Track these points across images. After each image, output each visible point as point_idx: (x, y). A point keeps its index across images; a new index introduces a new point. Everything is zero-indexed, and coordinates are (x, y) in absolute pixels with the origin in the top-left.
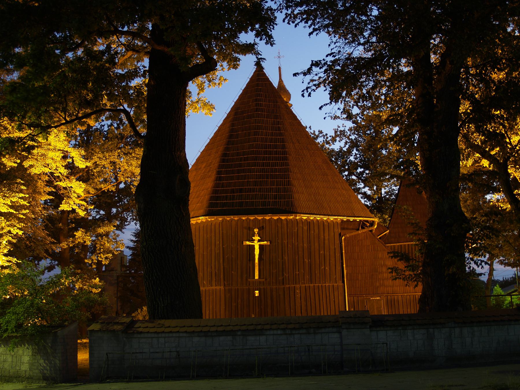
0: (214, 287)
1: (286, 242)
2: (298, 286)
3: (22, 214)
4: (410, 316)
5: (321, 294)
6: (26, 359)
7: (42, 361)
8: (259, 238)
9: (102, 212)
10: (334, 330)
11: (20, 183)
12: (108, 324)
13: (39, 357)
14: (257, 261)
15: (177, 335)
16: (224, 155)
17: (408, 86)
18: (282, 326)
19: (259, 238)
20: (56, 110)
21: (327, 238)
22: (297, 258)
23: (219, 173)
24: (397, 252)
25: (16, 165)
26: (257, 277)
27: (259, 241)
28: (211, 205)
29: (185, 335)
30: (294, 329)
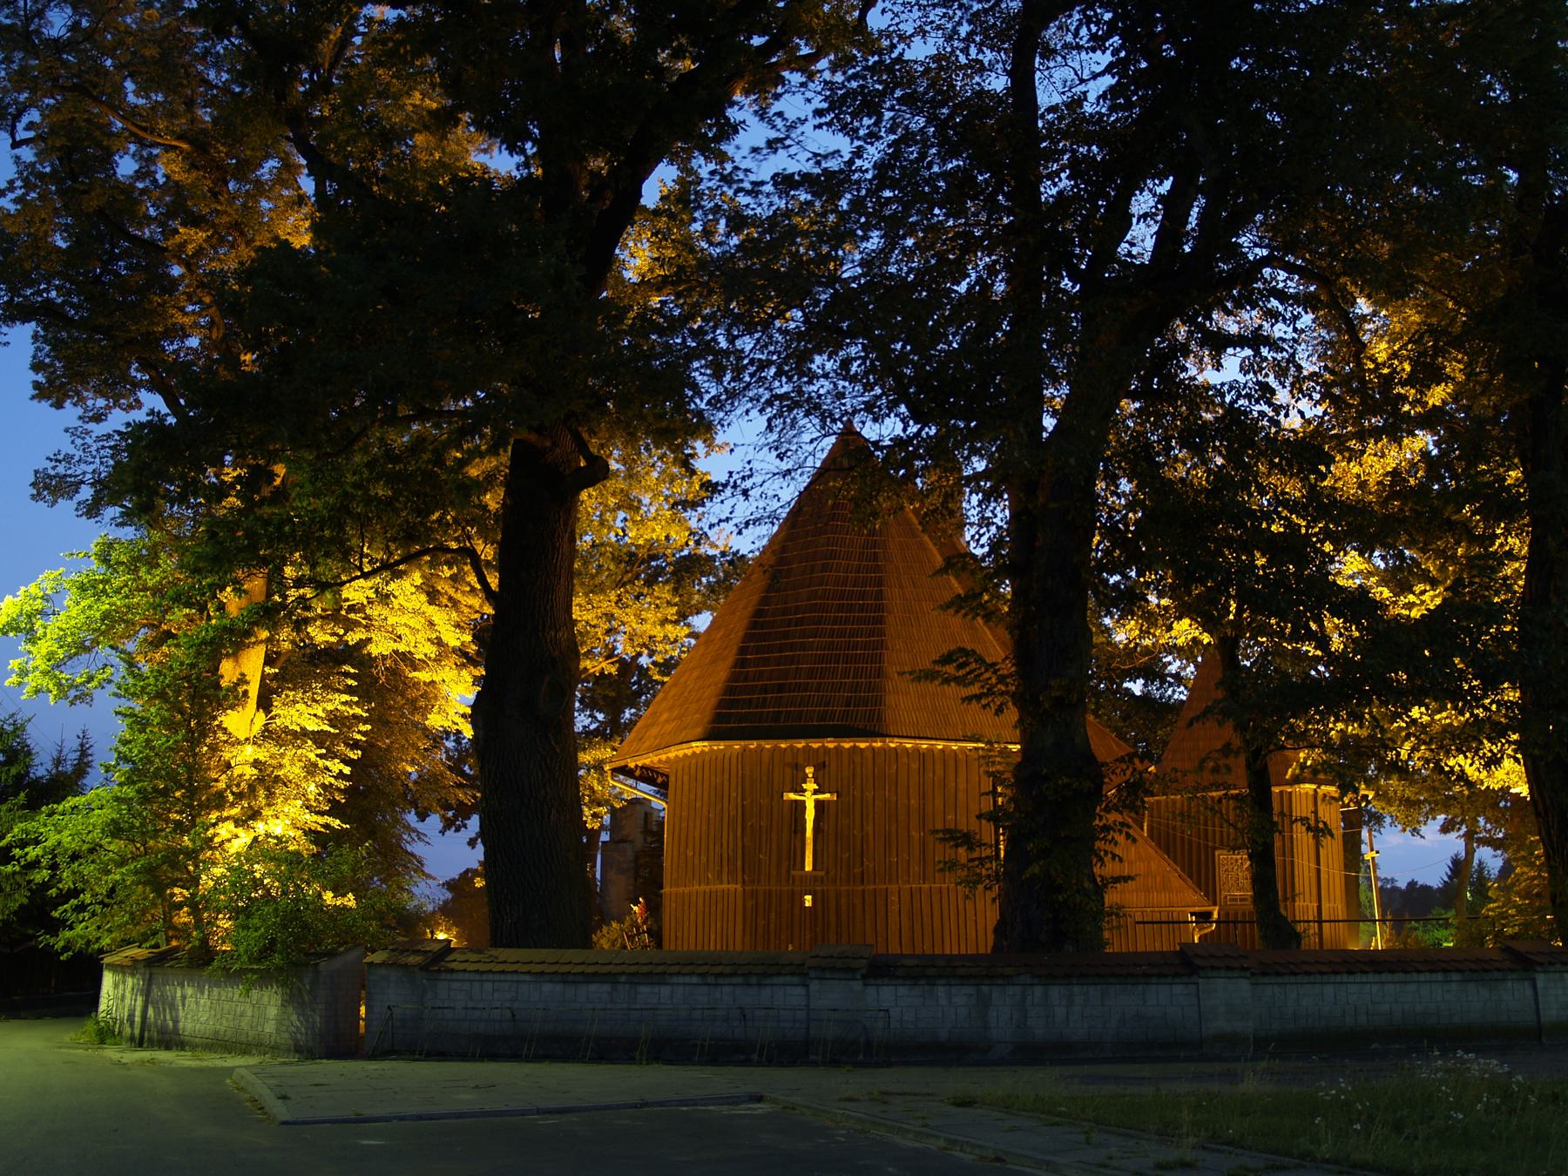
0: (725, 886)
1: (870, 795)
2: (893, 887)
3: (359, 732)
4: (974, 959)
5: (945, 906)
6: (273, 1012)
7: (294, 1017)
9: (600, 716)
10: (796, 980)
11: (347, 675)
12: (402, 952)
13: (290, 1009)
14: (809, 833)
15: (515, 977)
16: (758, 613)
20: (327, 555)
21: (962, 786)
22: (893, 828)
23: (742, 650)
24: (949, 831)
25: (334, 639)
26: (808, 867)
27: (815, 792)
28: (718, 718)
29: (527, 978)
30: (721, 975)
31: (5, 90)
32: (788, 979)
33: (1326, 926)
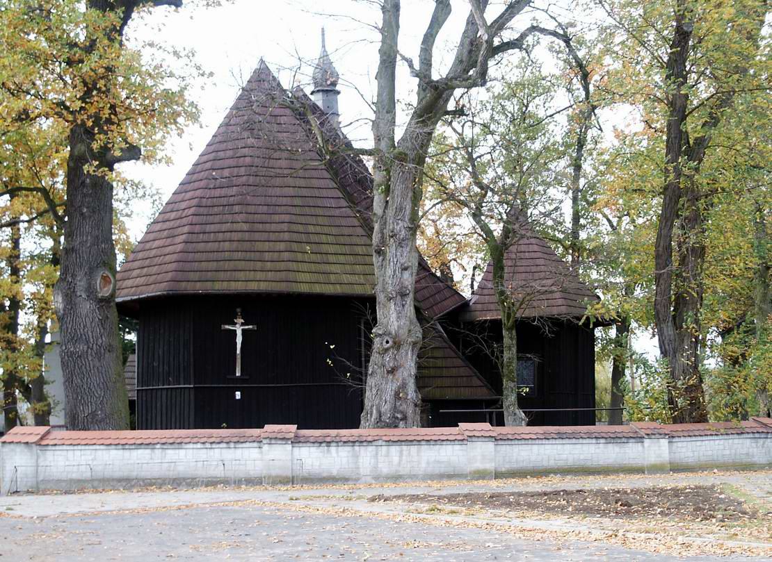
8: (243, 321)
14: (238, 351)
17: (372, 333)
18: (203, 440)
19: (243, 321)
26: (238, 374)
27: (243, 324)
29: (102, 447)
31: (741, 2)
32: (251, 445)
33: (39, 468)
